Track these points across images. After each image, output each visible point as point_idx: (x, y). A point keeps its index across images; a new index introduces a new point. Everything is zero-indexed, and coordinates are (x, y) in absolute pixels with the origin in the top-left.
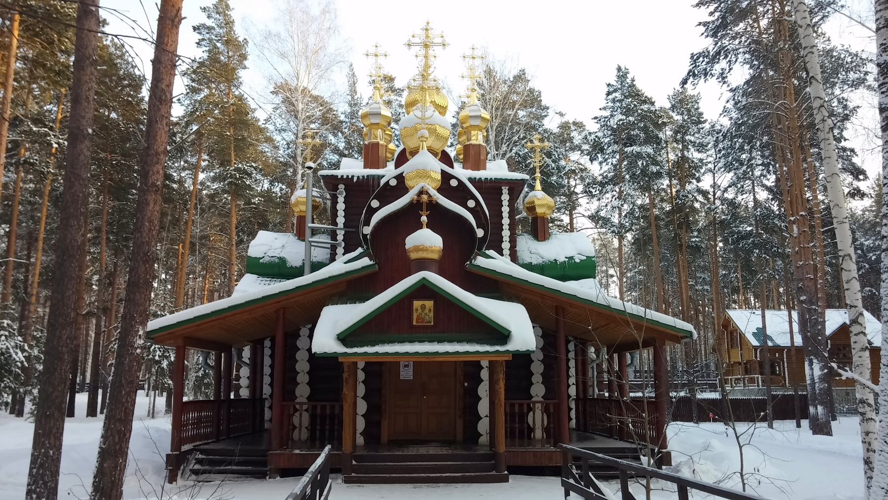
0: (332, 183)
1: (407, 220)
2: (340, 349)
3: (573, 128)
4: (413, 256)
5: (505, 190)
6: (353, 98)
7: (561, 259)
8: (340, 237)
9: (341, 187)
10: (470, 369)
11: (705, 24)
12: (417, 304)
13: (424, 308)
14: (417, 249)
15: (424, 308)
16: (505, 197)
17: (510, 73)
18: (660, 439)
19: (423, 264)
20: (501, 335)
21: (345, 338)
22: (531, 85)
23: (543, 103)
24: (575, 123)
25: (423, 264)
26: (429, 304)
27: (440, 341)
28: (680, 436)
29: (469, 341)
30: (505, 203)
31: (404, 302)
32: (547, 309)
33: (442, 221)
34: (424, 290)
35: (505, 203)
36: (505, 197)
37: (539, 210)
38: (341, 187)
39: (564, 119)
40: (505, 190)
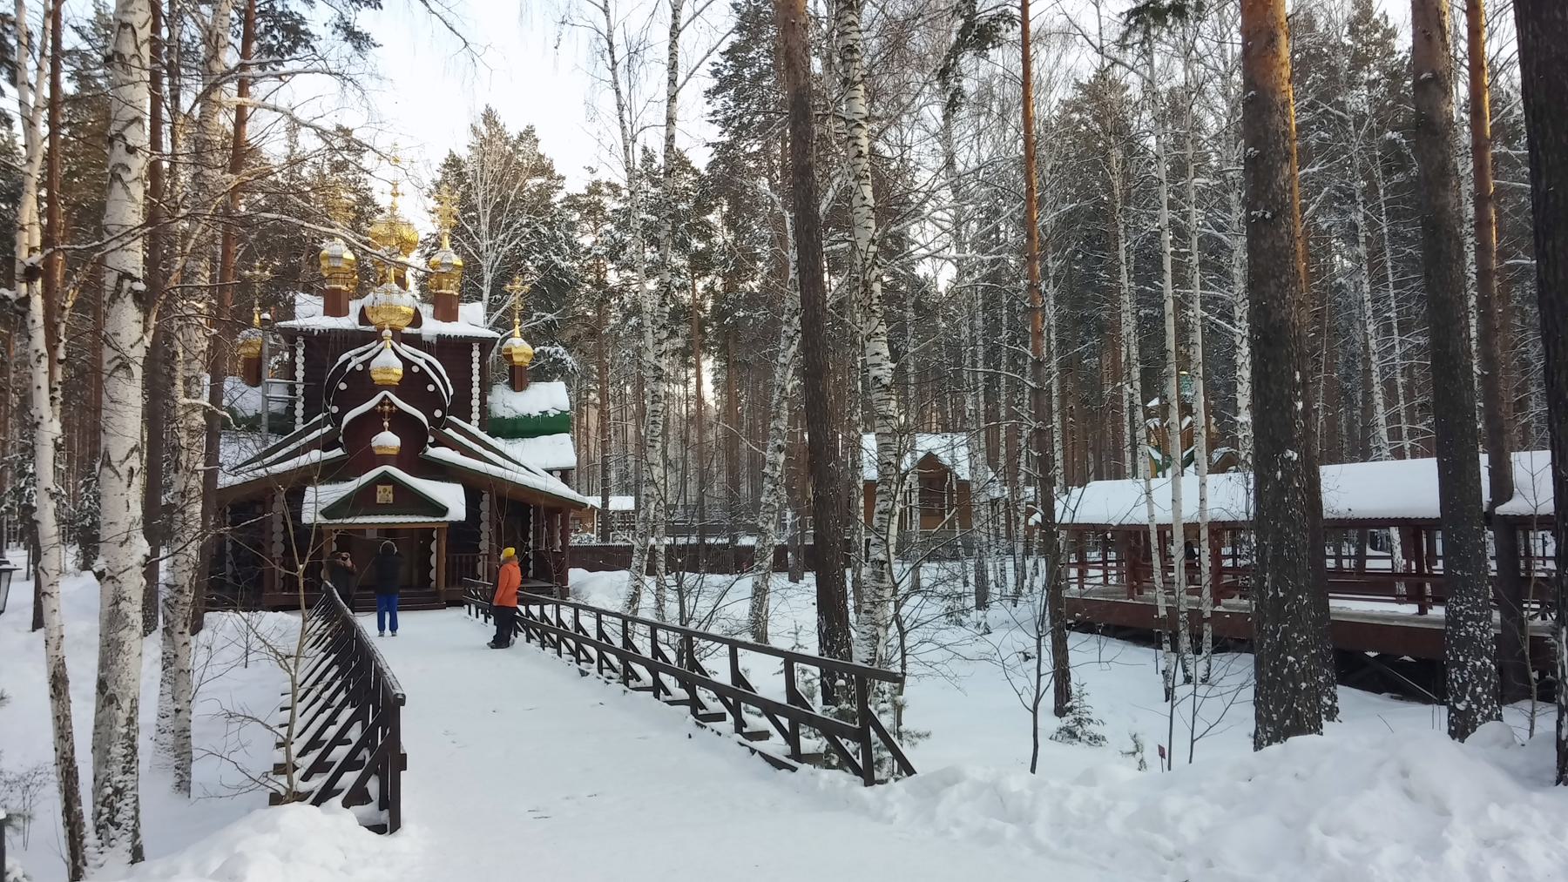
0: (291, 335)
1: (371, 423)
2: (321, 519)
3: (605, 191)
4: (377, 452)
5: (476, 347)
6: (292, 151)
7: (535, 413)
8: (300, 391)
9: (300, 340)
10: (426, 533)
11: (714, 145)
12: (380, 488)
13: (384, 494)
14: (380, 447)
15: (384, 494)
16: (476, 354)
17: (513, 130)
18: (564, 580)
19: (384, 459)
20: (443, 511)
21: (329, 512)
22: (541, 149)
23: (557, 173)
24: (609, 185)
25: (384, 459)
26: (390, 488)
27: (397, 514)
28: (576, 575)
29: (418, 514)
30: (476, 360)
31: (370, 488)
32: (475, 486)
33: (401, 423)
34: (386, 479)
35: (476, 360)
36: (476, 354)
37: (516, 359)
38: (300, 340)
39: (595, 178)
40: (476, 347)
